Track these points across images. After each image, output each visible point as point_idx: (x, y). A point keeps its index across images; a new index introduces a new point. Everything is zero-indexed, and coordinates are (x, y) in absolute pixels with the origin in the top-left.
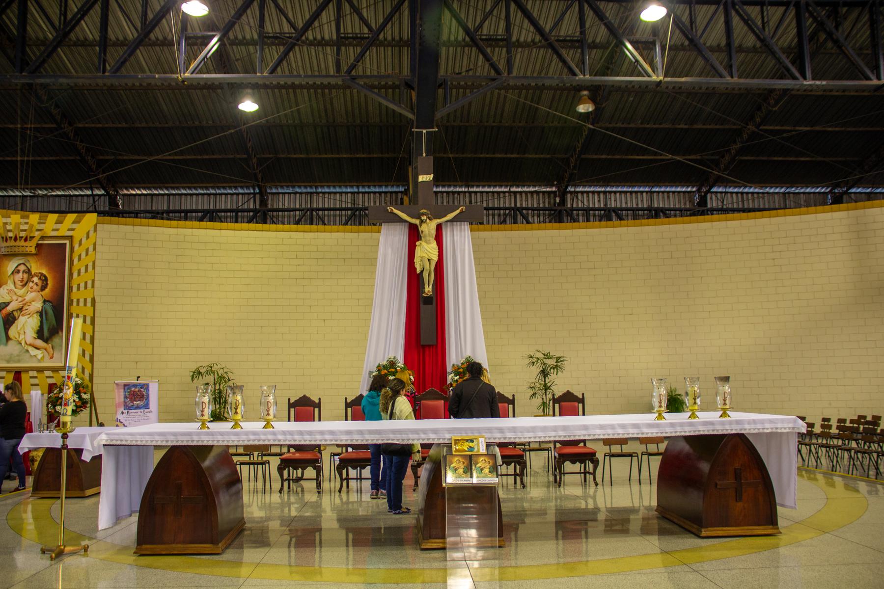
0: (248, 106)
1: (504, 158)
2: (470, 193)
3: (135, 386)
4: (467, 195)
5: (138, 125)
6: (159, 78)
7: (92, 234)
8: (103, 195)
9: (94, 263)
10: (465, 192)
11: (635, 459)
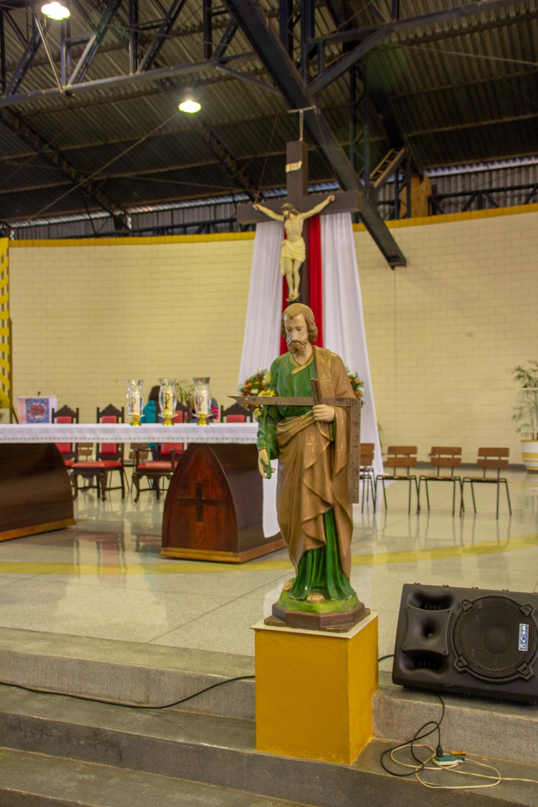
0: (190, 106)
1: (518, 122)
2: (491, 171)
3: (36, 401)
4: (487, 174)
5: (111, 141)
6: (47, 94)
7: (6, 258)
8: (107, 218)
9: (8, 286)
10: (483, 172)
11: (413, 482)
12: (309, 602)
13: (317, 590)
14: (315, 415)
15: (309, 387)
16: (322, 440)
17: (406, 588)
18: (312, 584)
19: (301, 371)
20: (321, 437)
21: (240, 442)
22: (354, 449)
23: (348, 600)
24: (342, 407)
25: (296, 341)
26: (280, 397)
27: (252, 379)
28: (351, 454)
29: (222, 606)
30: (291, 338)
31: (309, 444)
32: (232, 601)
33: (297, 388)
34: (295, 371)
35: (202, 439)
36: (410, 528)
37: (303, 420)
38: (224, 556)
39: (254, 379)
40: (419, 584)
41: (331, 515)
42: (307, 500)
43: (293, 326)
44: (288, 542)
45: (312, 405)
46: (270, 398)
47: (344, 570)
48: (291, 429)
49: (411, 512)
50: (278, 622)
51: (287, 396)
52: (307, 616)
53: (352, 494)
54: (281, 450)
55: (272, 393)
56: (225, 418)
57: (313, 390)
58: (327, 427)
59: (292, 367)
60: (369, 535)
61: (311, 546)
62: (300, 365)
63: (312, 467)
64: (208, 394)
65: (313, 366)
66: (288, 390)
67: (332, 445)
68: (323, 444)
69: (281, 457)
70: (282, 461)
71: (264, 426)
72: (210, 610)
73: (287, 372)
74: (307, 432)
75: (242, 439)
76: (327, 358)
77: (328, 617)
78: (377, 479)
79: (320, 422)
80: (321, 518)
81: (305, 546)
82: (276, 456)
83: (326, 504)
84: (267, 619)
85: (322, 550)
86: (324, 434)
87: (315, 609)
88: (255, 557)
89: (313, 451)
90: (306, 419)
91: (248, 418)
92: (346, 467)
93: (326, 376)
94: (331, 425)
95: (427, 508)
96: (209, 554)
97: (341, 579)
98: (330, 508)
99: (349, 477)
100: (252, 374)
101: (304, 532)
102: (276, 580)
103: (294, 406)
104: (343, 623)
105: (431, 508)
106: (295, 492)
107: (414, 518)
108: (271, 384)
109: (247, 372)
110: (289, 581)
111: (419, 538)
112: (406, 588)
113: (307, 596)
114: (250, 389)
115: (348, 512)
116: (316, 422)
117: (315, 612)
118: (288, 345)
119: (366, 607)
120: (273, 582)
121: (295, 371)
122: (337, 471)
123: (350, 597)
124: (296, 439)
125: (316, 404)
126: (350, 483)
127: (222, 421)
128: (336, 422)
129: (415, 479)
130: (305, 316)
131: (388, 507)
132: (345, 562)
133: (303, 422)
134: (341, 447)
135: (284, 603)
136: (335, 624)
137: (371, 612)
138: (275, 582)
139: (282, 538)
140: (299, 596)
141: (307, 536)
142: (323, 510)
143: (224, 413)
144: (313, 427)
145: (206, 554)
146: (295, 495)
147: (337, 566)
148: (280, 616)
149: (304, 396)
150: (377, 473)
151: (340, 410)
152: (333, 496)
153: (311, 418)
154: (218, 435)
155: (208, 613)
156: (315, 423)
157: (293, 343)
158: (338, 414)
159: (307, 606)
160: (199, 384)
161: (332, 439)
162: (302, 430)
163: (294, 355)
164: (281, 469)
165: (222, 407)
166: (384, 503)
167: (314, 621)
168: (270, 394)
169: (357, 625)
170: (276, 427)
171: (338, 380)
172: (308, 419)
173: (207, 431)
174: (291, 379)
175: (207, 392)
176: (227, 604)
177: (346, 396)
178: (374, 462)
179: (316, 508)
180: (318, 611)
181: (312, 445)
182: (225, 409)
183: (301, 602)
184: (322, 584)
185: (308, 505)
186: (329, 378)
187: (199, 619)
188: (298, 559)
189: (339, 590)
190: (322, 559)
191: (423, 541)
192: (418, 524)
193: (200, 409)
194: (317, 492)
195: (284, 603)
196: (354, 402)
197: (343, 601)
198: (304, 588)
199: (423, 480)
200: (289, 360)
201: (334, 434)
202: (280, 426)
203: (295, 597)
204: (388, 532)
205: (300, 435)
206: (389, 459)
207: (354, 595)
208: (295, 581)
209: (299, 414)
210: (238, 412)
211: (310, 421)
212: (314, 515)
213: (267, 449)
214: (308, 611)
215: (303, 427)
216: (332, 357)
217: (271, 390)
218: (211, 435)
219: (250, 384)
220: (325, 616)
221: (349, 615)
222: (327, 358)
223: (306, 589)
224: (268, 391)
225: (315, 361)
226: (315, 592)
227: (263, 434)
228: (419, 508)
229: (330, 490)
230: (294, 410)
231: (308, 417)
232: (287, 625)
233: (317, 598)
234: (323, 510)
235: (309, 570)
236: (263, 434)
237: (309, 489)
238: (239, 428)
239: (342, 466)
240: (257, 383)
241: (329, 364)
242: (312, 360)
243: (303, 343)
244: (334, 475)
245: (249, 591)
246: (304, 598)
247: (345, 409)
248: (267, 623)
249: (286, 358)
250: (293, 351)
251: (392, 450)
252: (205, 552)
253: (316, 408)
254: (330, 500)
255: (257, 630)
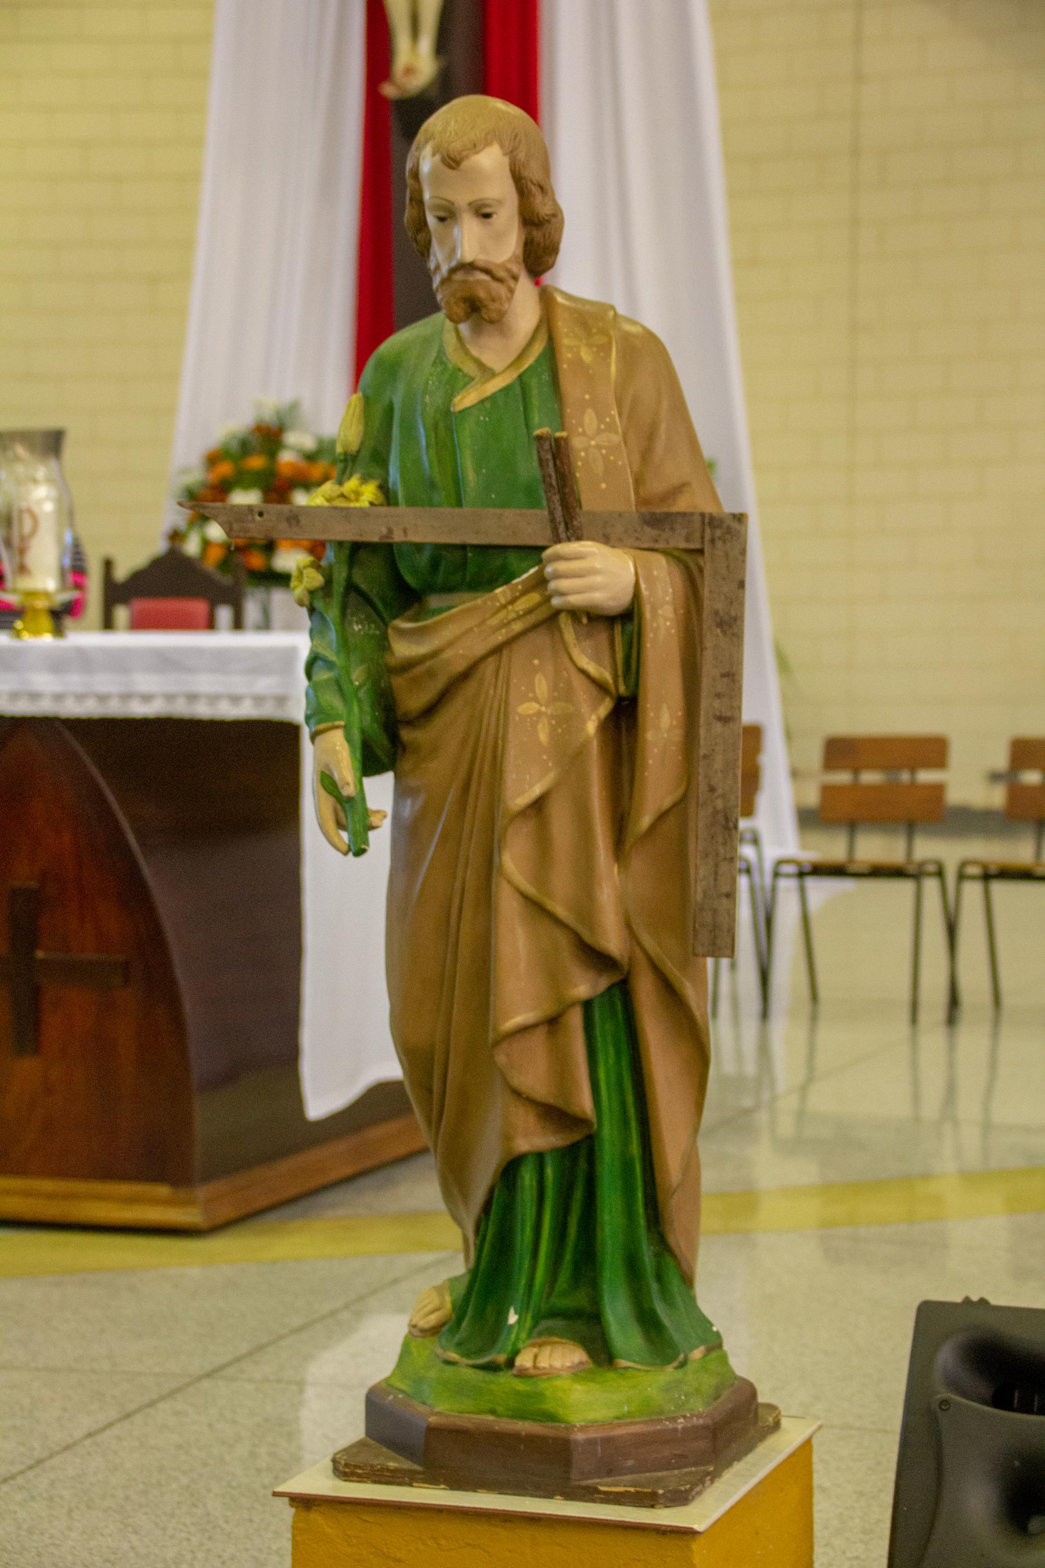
11: (931, 886)
12: (523, 1375)
13: (559, 1323)
14: (553, 585)
15: (528, 467)
16: (582, 690)
17: (930, 1317)
18: (535, 1298)
19: (492, 398)
20: (579, 683)
21: (203, 711)
22: (718, 727)
23: (689, 1367)
24: (665, 553)
25: (470, 267)
26: (402, 509)
27: (235, 446)
28: (703, 751)
29: (128, 1416)
30: (453, 251)
31: (528, 708)
32: (172, 1394)
33: (477, 472)
34: (466, 399)
35: (35, 696)
36: (916, 1084)
37: (503, 606)
38: (130, 1200)
39: (244, 447)
40: (983, 1302)
41: (619, 1006)
42: (516, 943)
43: (461, 198)
44: (434, 1121)
45: (540, 543)
46: (363, 513)
47: (671, 1240)
48: (451, 644)
49: (924, 1017)
50: (392, 1465)
51: (431, 505)
52: (516, 1437)
53: (708, 917)
54: (406, 734)
55: (369, 492)
56: (122, 614)
57: (545, 478)
58: (602, 637)
59: (455, 381)
60: (748, 1112)
61: (533, 1138)
62: (488, 373)
63: (539, 805)
64: (59, 501)
65: (546, 377)
66: (438, 478)
67: (625, 715)
68: (585, 709)
69: (406, 765)
70: (413, 782)
71: (333, 635)
72: (78, 1434)
73: (432, 401)
74: (518, 655)
75: (213, 699)
76: (602, 340)
77: (607, 1441)
78: (776, 875)
79: (574, 614)
80: (575, 1019)
81: (507, 1138)
82: (385, 760)
83: (597, 958)
84: (345, 1450)
85: (580, 1154)
86: (591, 668)
87: (549, 1406)
88: (264, 1202)
89: (543, 736)
90: (512, 601)
91: (224, 614)
92: (681, 804)
93: (600, 419)
94: (618, 629)
95: (987, 998)
96: (67, 1196)
97: (659, 1278)
98: (616, 978)
99: (695, 848)
100: (229, 423)
101: (504, 1079)
102: (361, 1298)
103: (463, 547)
104: (667, 1466)
105: (1007, 1000)
106: (468, 914)
107: (933, 1038)
108: (365, 453)
109: (208, 417)
110: (439, 1290)
111: (956, 1122)
112: (930, 1317)
113: (516, 1352)
114: (222, 489)
115: (690, 992)
116: (556, 613)
117: (550, 1417)
118: (436, 281)
119: (761, 1399)
120: (346, 1307)
121: (466, 399)
122: (646, 821)
123: (697, 1354)
124: (470, 688)
125: (558, 540)
126: (700, 872)
127: (108, 624)
128: (641, 616)
129: (940, 874)
130: (511, 154)
131: (823, 993)
132: (674, 1206)
133: (502, 614)
134: (661, 723)
135: (418, 1381)
136: (631, 1471)
137: (784, 1422)
138: (357, 1307)
139: (410, 1110)
140: (481, 1351)
141: (517, 1093)
142: (584, 986)
143: (116, 593)
144: (541, 639)
145: (51, 1196)
146: (466, 929)
147: (642, 1222)
148: (399, 1438)
149: (504, 505)
150: (772, 852)
151: (661, 567)
152: (628, 926)
153: (535, 598)
154: (105, 683)
155: (67, 1448)
156: (552, 618)
157: (459, 276)
158: (651, 580)
159: (518, 1393)
160: (17, 459)
161: (622, 689)
162: (497, 650)
163: (464, 328)
164: (407, 812)
165: (108, 565)
166: (803, 978)
167: (545, 1458)
168: (358, 494)
169: (727, 1475)
170: (385, 637)
171: (651, 436)
172: (522, 605)
173: (58, 664)
174: (449, 429)
175: (54, 493)
176: (152, 1404)
177: (681, 505)
178: (763, 801)
179: (554, 979)
180: (560, 1412)
181: (539, 714)
182: (121, 573)
183: (488, 1376)
184: (580, 1300)
185: (522, 967)
186: (611, 428)
187: (30, 1474)
188: (479, 1194)
189: (649, 1323)
190: (578, 1194)
191: (970, 1137)
192: (951, 1066)
193: (22, 569)
194: (561, 911)
195: (418, 1381)
196: (718, 533)
197: (670, 1369)
198: (502, 1315)
199: (973, 878)
200: (441, 352)
201: (631, 665)
202: (402, 633)
203: (467, 1355)
204: (823, 1100)
205: (489, 668)
206: (827, 791)
207: (715, 1344)
208: (461, 1289)
209: (484, 583)
210: (169, 589)
211: (529, 611)
212: (547, 1009)
213: (347, 729)
214: (522, 1415)
215: (500, 637)
216: (627, 337)
217: (364, 480)
218: (75, 682)
219: (225, 469)
220: (592, 1435)
221: (692, 1433)
222: (602, 340)
223: (513, 1318)
224: (352, 483)
225: (551, 353)
226: (550, 1332)
227: (330, 665)
228: (954, 1001)
229: (614, 902)
230: (464, 565)
231: (524, 593)
232: (434, 1473)
233: (561, 1357)
234: (584, 986)
235: (524, 1237)
236: (330, 665)
237: (526, 898)
238: (199, 652)
239: (667, 803)
240: (257, 462)
241: (613, 368)
242: (538, 348)
243: (502, 274)
244: (630, 840)
245: (244, 1348)
246: (502, 1358)
247: (679, 560)
248: (345, 1468)
249: (426, 342)
250: (459, 310)
251: (840, 751)
252: (48, 1185)
253: (558, 558)
254: (613, 942)
255: (304, 1503)
